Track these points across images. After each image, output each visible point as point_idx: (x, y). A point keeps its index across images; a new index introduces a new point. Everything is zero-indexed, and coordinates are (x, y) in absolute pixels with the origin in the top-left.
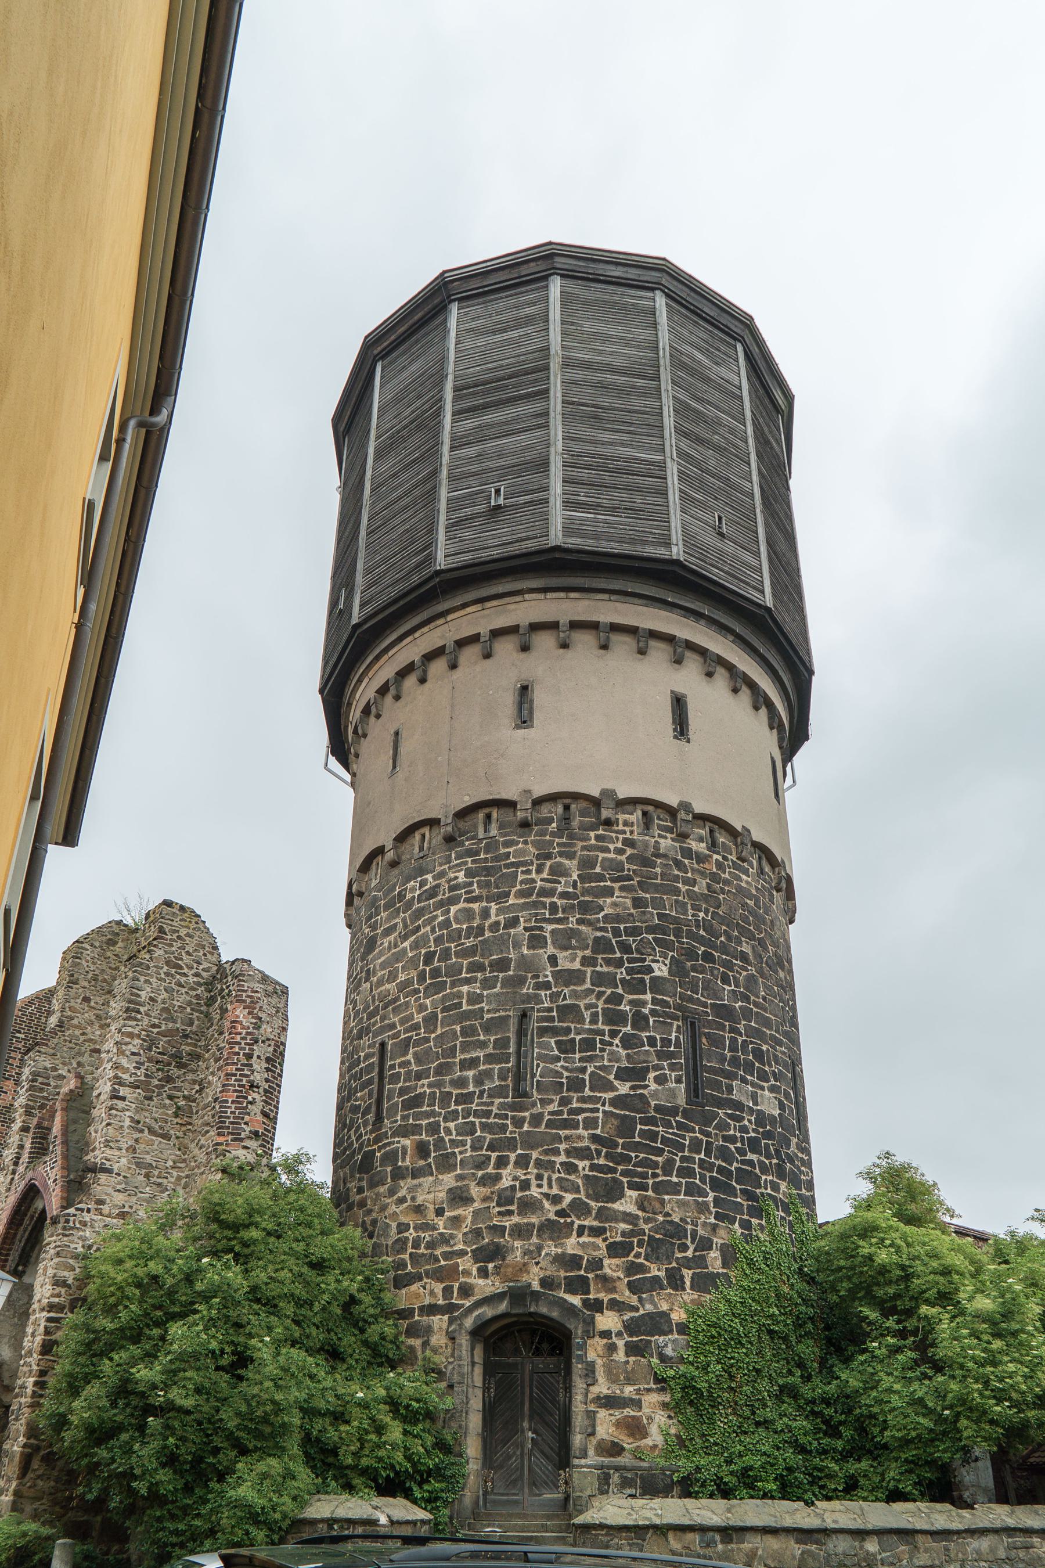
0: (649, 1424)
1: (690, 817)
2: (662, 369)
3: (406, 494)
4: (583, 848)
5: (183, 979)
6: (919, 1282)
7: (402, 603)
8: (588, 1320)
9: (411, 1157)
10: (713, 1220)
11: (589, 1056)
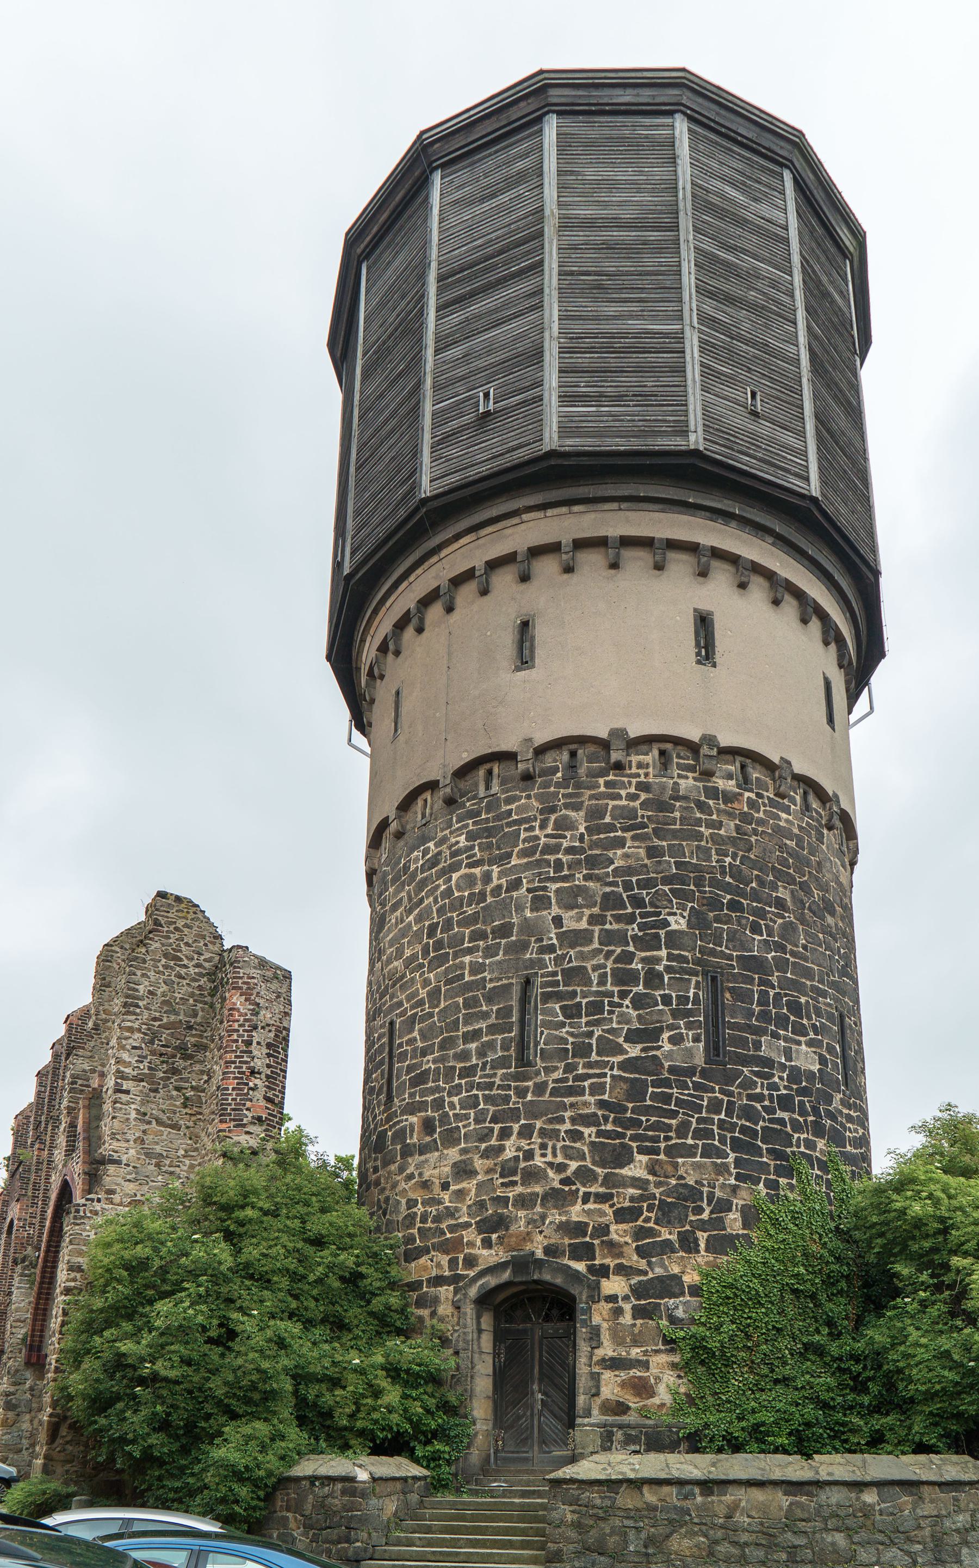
0: (656, 1383)
1: (714, 752)
2: (681, 214)
3: (392, 416)
4: (592, 797)
5: (183, 971)
6: (957, 1233)
7: (391, 543)
8: (593, 1285)
9: (418, 1134)
10: (733, 1182)
11: (596, 1020)
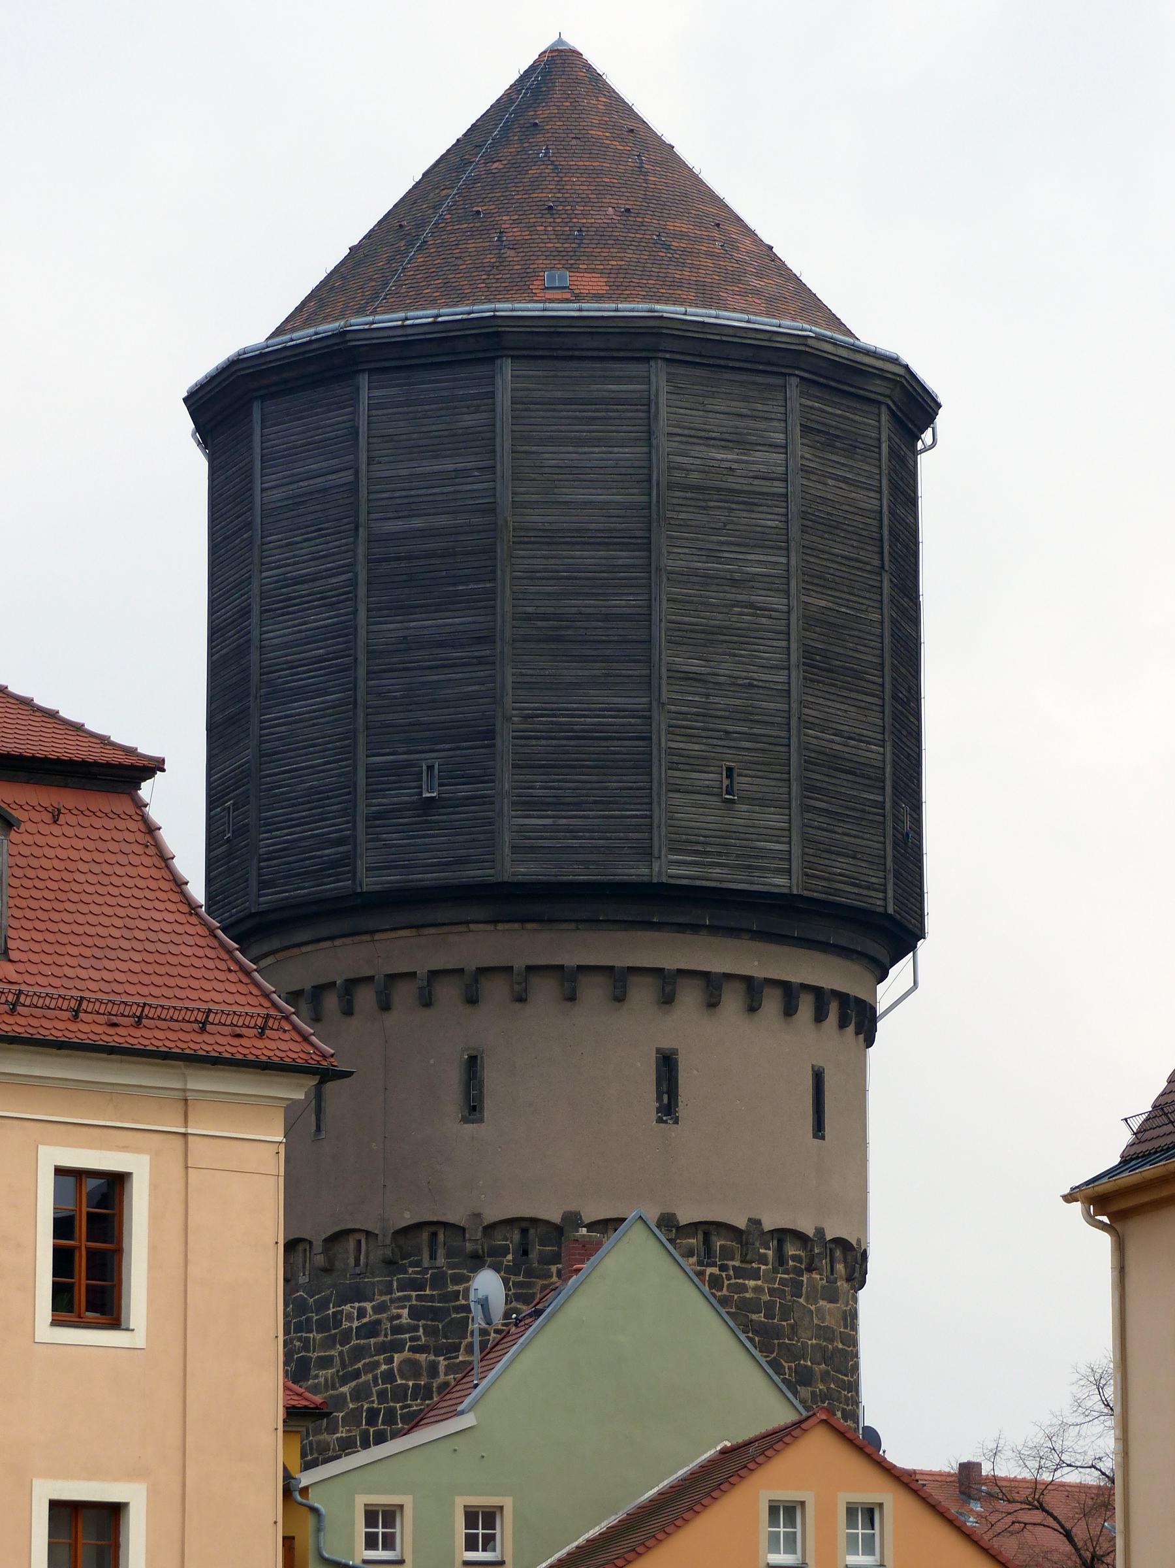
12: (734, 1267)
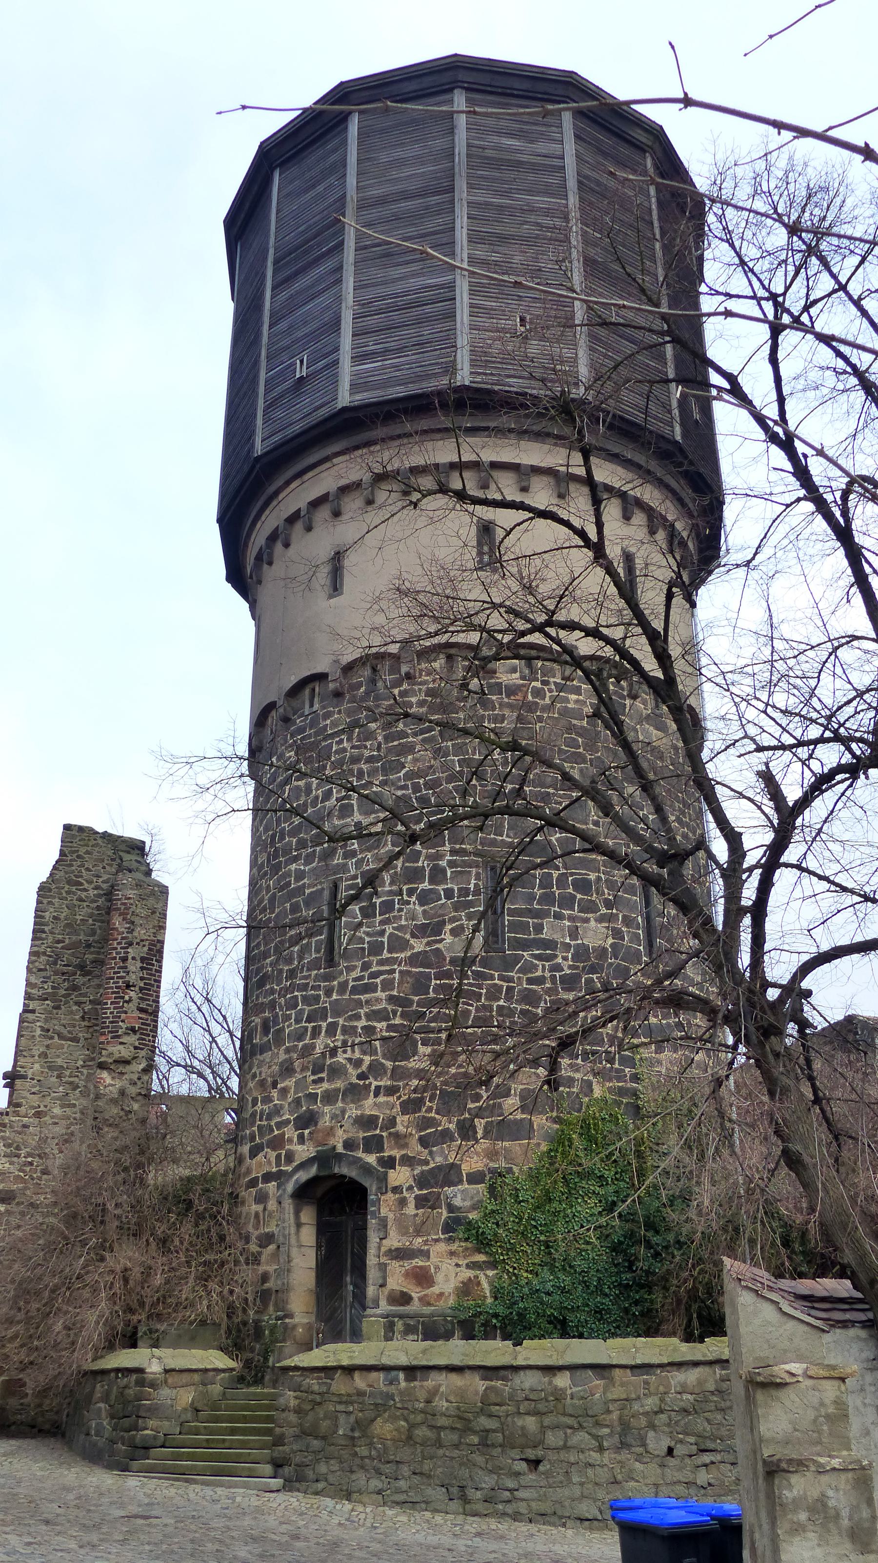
0: (436, 1273)
2: (457, 177)
5: (83, 895)
12: (555, 683)
